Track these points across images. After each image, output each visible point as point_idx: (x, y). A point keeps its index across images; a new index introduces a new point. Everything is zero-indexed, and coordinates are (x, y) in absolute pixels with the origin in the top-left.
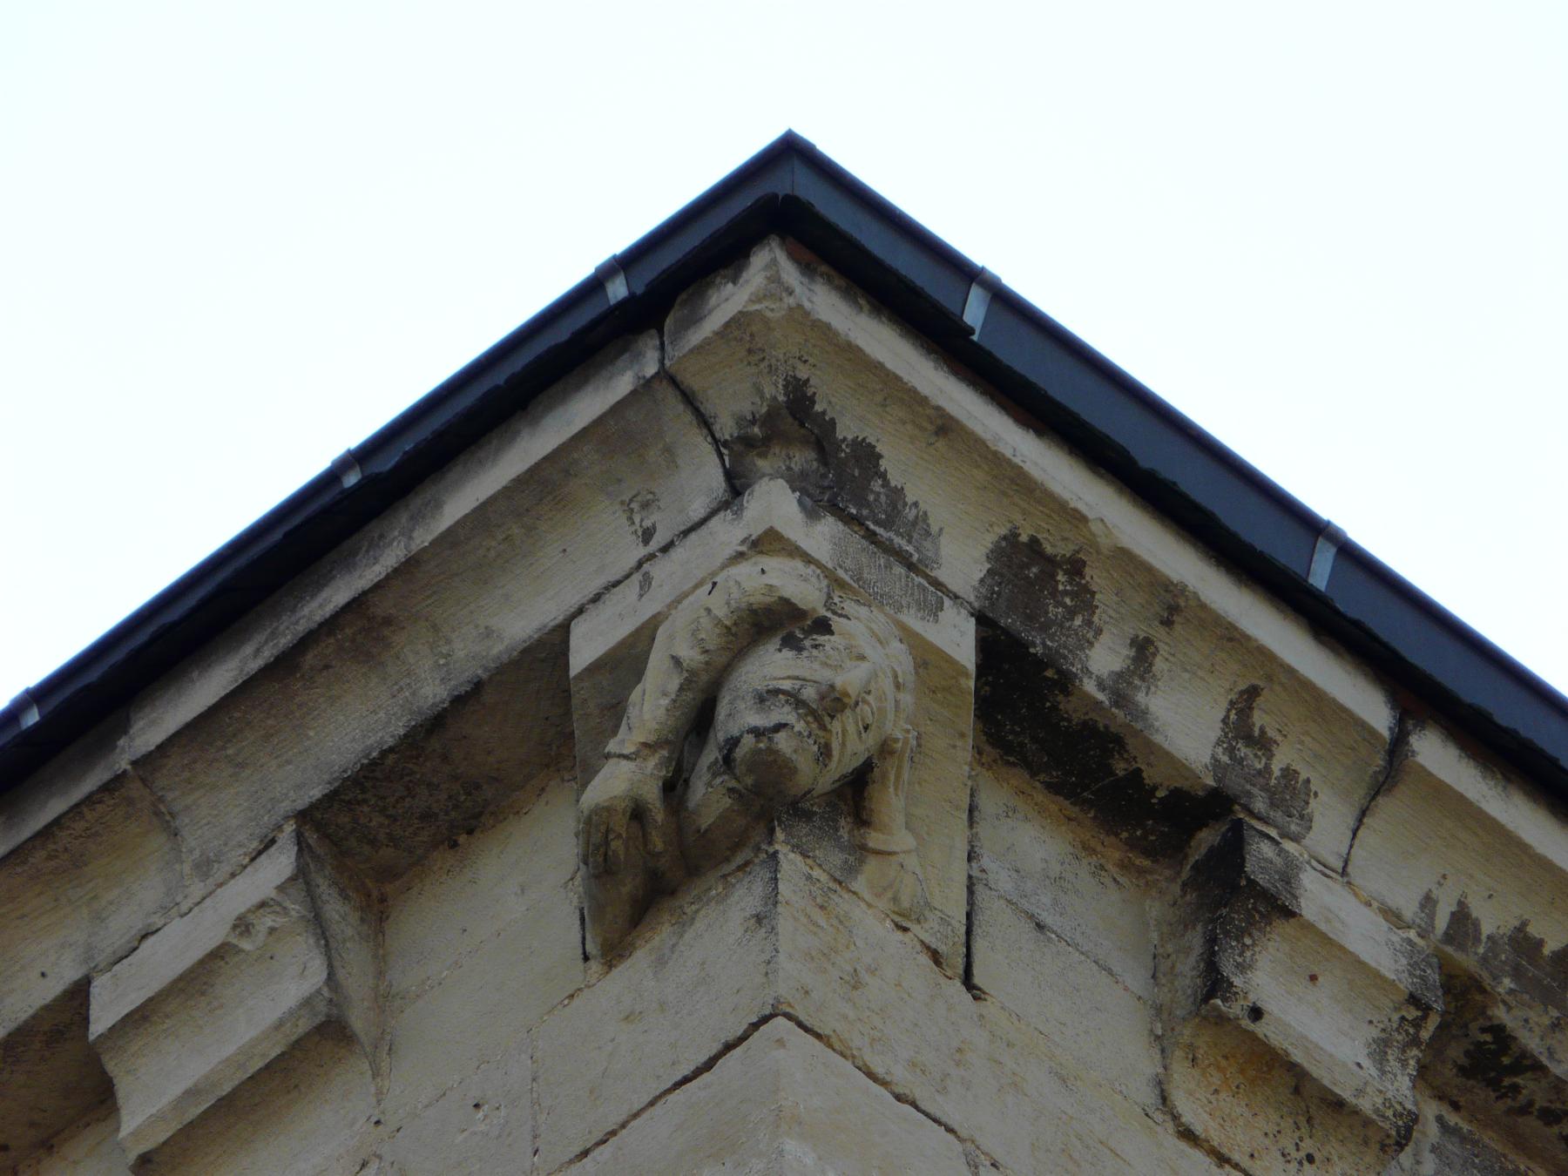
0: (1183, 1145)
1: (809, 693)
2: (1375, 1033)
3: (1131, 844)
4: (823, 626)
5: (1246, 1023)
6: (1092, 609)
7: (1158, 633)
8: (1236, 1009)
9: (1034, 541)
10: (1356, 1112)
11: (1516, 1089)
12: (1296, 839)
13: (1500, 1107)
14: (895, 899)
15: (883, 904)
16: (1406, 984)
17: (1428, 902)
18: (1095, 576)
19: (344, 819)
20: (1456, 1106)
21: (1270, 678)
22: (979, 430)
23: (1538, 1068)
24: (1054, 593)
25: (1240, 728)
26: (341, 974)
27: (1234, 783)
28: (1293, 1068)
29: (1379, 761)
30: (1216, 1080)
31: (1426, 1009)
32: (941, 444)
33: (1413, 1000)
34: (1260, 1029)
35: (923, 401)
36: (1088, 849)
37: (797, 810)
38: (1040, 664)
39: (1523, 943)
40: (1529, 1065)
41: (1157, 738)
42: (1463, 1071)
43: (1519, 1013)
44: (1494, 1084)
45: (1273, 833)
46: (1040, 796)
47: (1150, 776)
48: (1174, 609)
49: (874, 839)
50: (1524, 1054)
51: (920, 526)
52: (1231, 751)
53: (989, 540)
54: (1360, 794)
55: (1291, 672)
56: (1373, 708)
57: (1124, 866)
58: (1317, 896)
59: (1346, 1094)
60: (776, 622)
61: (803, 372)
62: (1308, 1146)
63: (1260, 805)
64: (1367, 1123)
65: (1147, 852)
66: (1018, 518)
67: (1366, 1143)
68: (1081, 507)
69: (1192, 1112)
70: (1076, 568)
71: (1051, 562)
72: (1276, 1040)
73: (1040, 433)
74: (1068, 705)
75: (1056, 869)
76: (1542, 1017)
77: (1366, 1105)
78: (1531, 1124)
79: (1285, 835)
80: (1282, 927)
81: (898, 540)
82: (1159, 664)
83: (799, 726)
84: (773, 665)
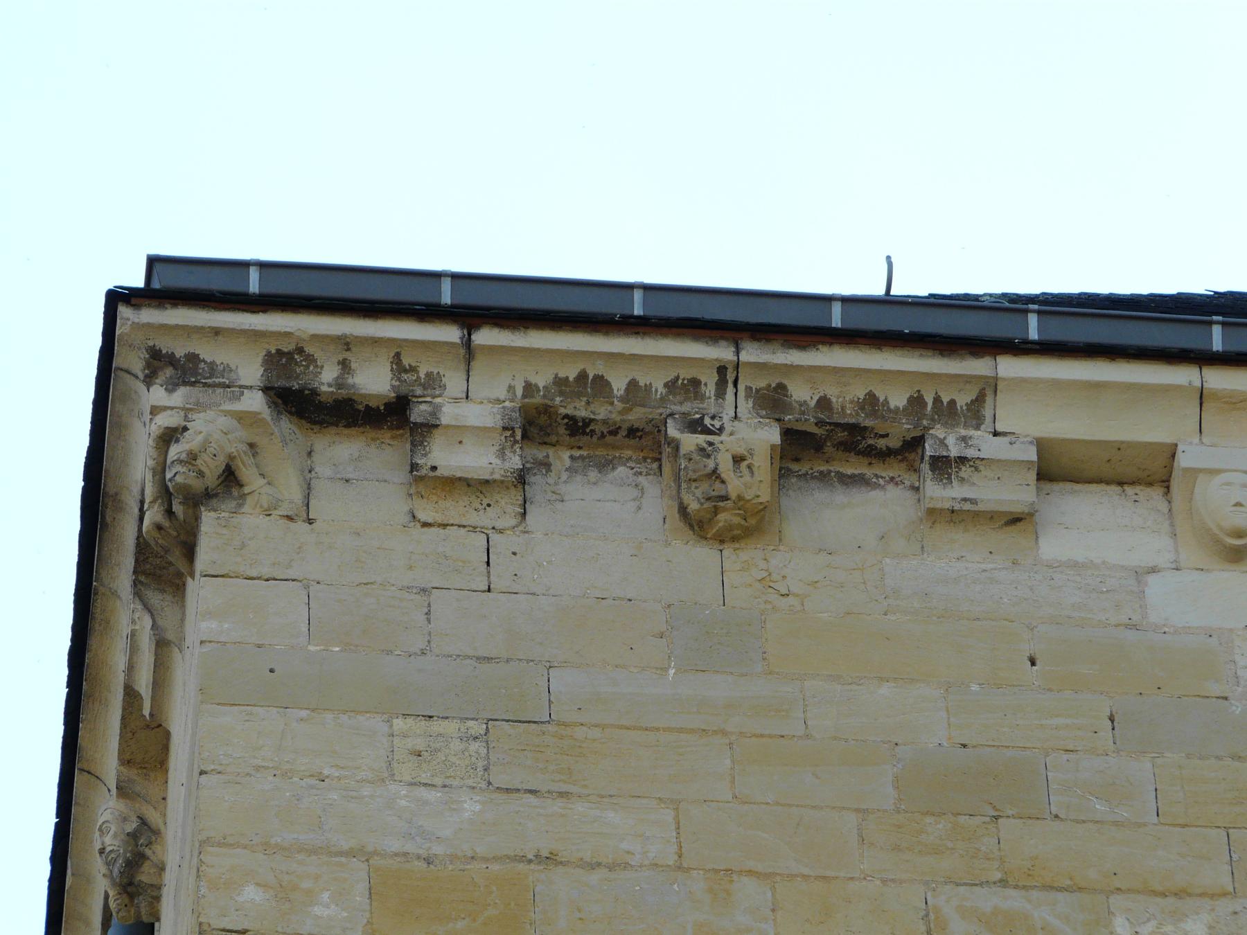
0: (425, 529)
1: (184, 456)
2: (497, 448)
3: (390, 428)
4: (185, 429)
5: (432, 474)
6: (315, 361)
7: (347, 355)
8: (424, 472)
9: (278, 351)
10: (495, 481)
11: (593, 431)
12: (440, 396)
13: (595, 439)
14: (261, 507)
15: (258, 510)
16: (500, 424)
17: (511, 388)
18: (309, 349)
19: (148, 566)
20: (580, 448)
21: (399, 346)
22: (231, 326)
23: (592, 420)
24: (296, 363)
25: (399, 368)
26: (160, 622)
27: (404, 390)
28: (460, 479)
29: (462, 351)
30: (435, 498)
31: (513, 429)
32: (220, 338)
33: (505, 429)
34: (438, 473)
35: (202, 328)
36: (373, 439)
37: (208, 496)
38: (301, 391)
39: (560, 382)
40: (587, 422)
41: (363, 391)
42: (571, 435)
43: (571, 406)
44: (584, 433)
45: (428, 399)
46: (346, 431)
47: (373, 404)
48: (347, 344)
49: (246, 490)
50: (584, 420)
51: (228, 369)
52: (399, 379)
53: (260, 359)
54: (463, 366)
55: (406, 340)
56: (450, 333)
57: (393, 438)
58: (449, 413)
59: (487, 477)
60: (169, 437)
61: (151, 343)
62: (485, 502)
63: (419, 391)
64: (502, 482)
65: (398, 428)
66: (267, 346)
67: (508, 488)
68: (288, 330)
69: (423, 516)
70: (300, 350)
71: (289, 355)
72: (446, 473)
73: (264, 311)
74: (323, 399)
75: (356, 454)
76: (581, 403)
77: (497, 476)
78: (609, 439)
79: (434, 397)
80: (436, 432)
81: (217, 380)
82: (353, 365)
83: (184, 469)
84: (174, 451)
